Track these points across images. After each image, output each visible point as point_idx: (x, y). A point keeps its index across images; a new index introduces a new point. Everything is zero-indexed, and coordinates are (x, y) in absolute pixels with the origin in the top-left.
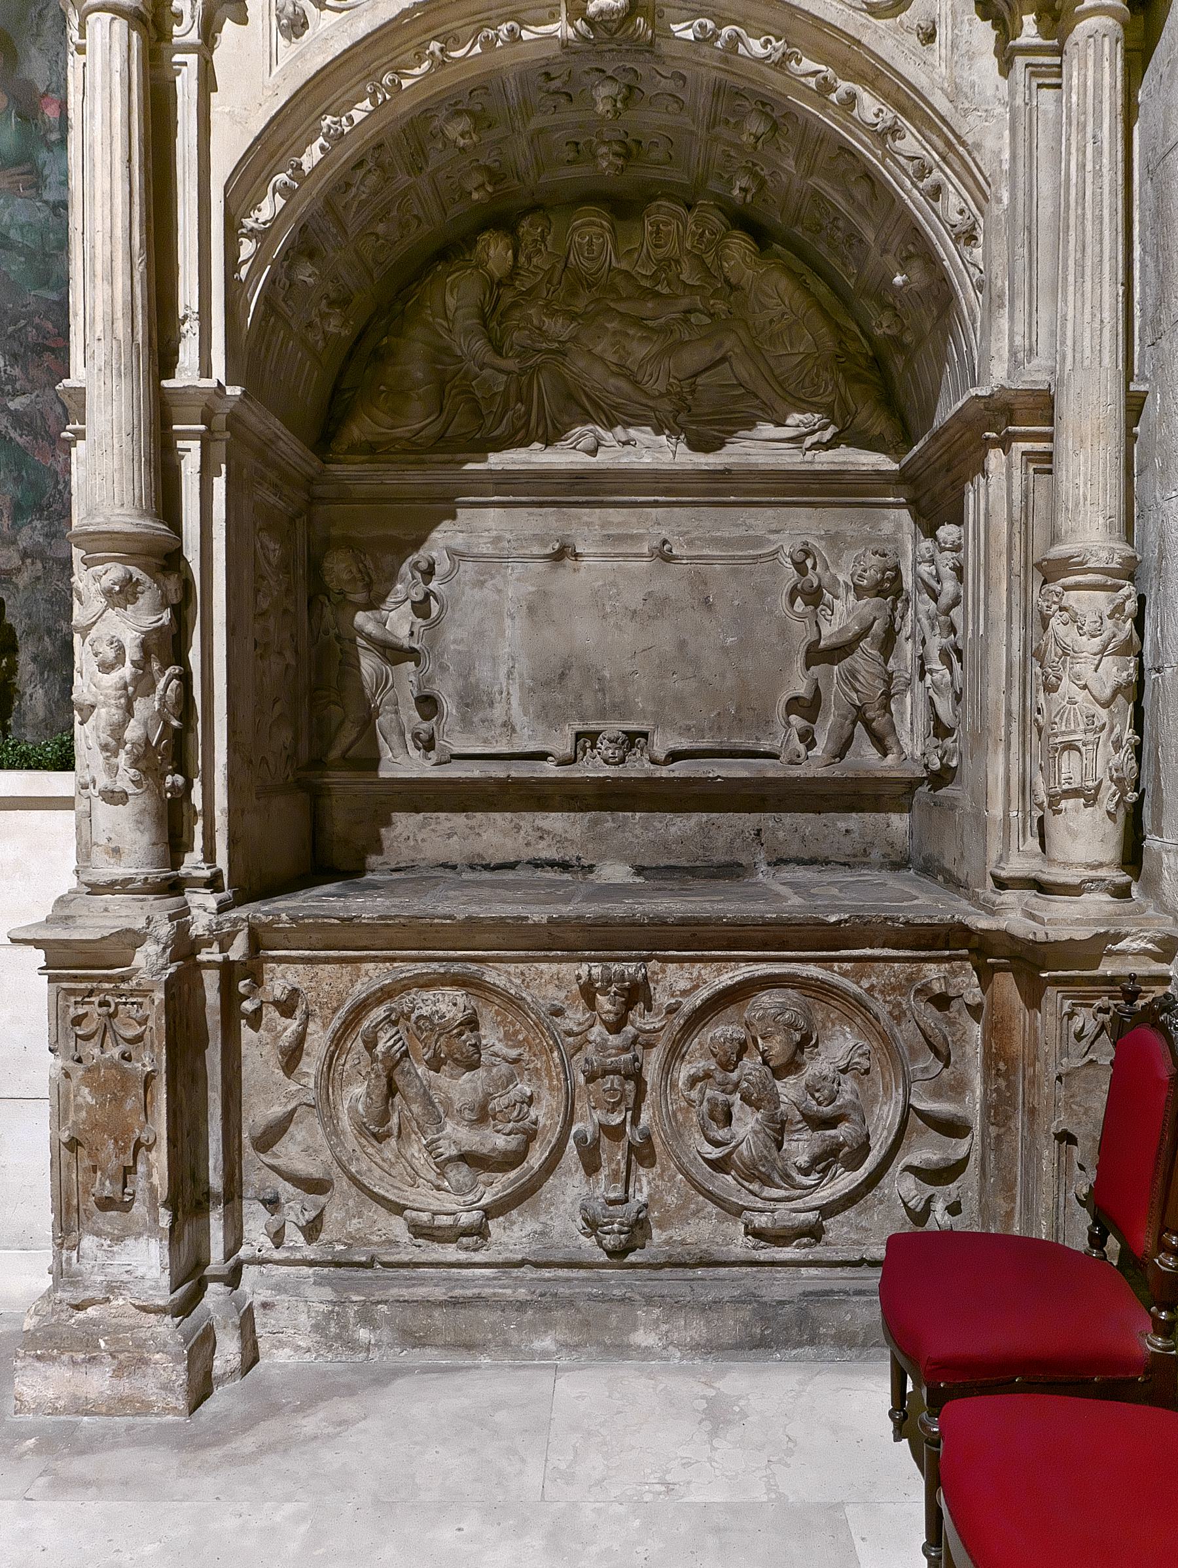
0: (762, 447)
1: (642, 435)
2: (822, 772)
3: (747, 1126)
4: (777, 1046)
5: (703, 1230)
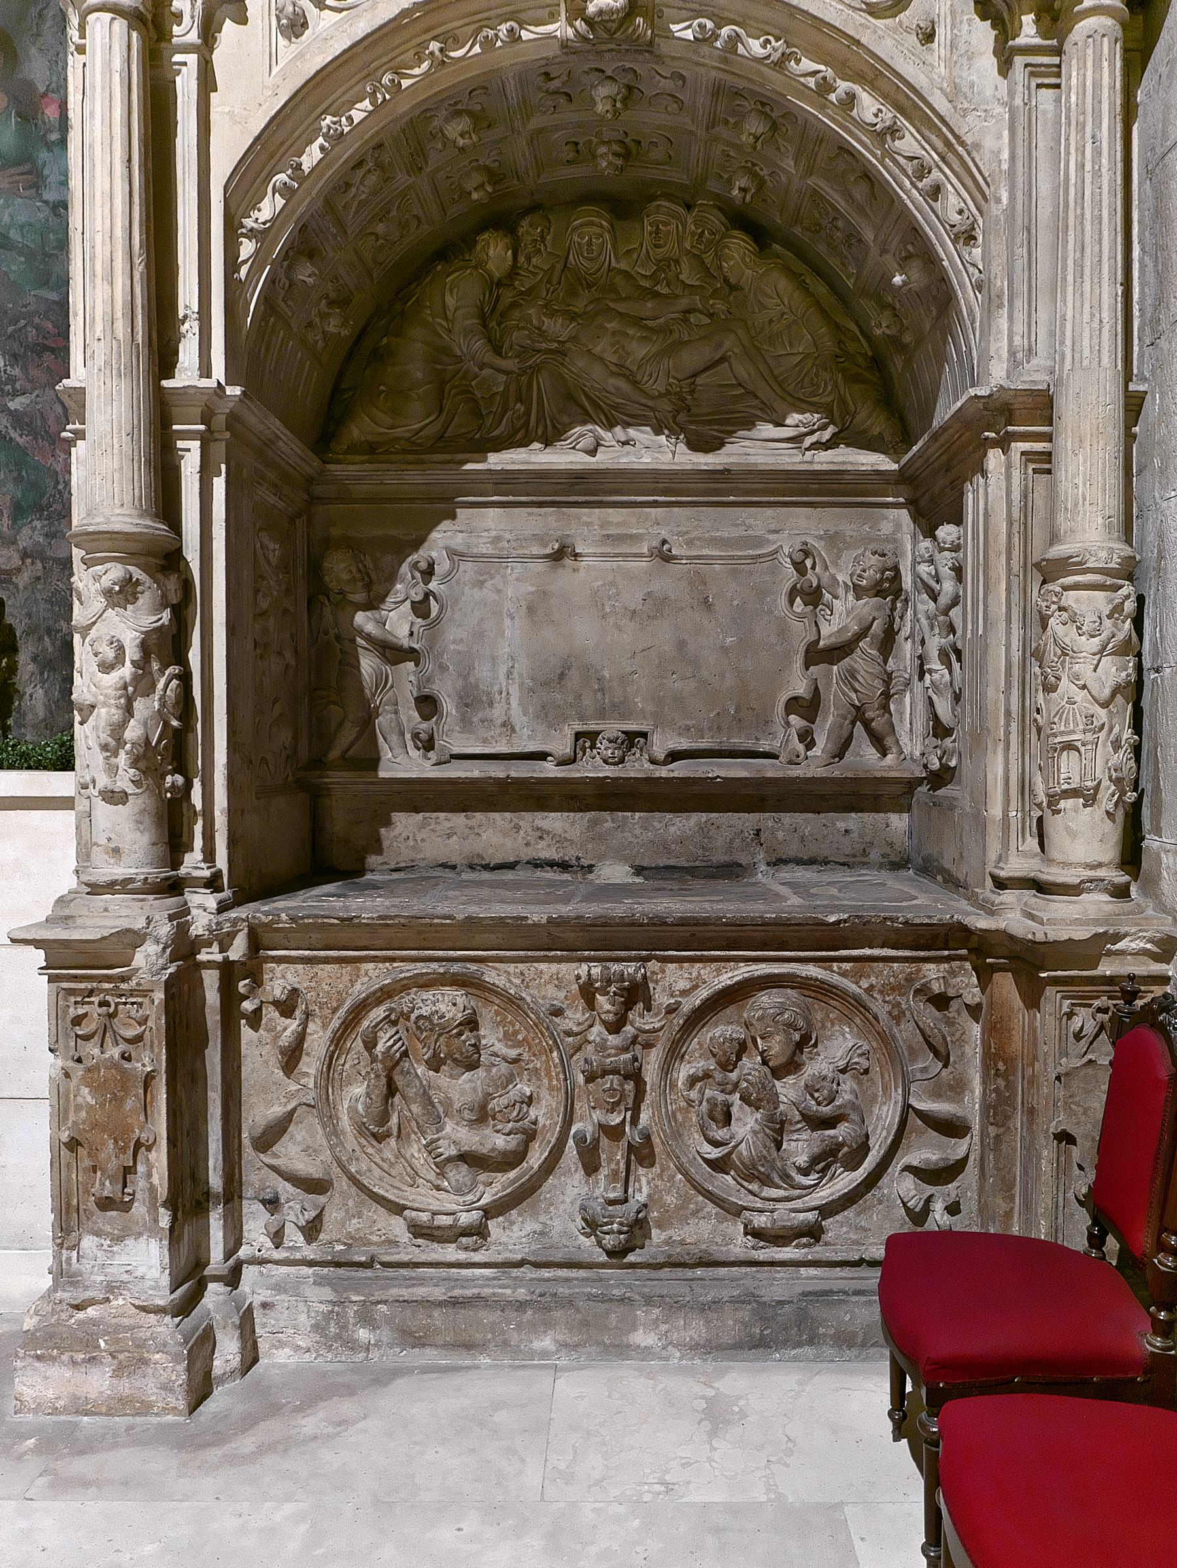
0: (762, 447)
1: (642, 435)
2: (821, 772)
3: (746, 1126)
4: (777, 1046)
5: (703, 1230)
